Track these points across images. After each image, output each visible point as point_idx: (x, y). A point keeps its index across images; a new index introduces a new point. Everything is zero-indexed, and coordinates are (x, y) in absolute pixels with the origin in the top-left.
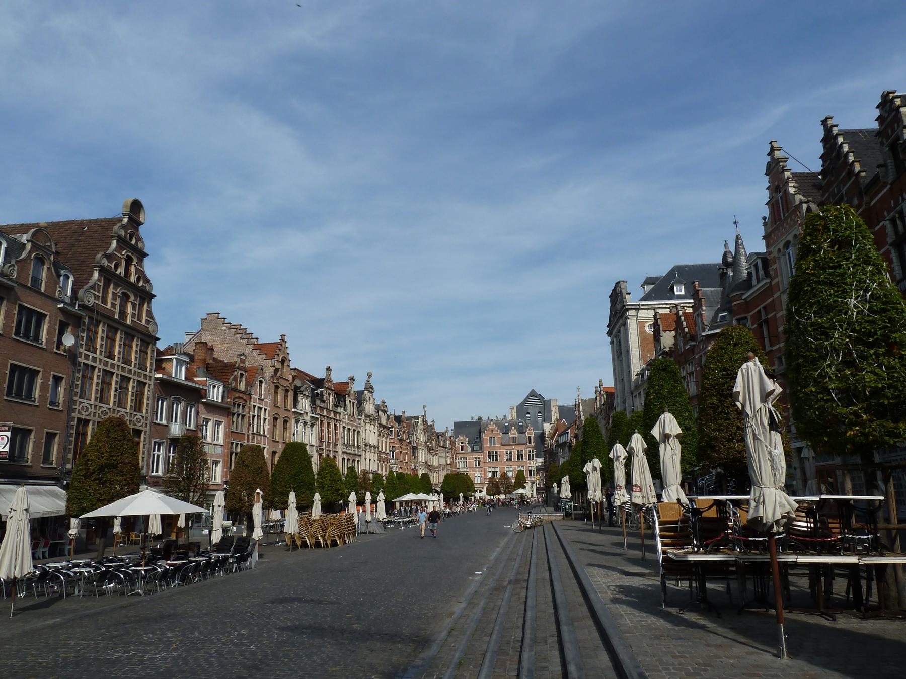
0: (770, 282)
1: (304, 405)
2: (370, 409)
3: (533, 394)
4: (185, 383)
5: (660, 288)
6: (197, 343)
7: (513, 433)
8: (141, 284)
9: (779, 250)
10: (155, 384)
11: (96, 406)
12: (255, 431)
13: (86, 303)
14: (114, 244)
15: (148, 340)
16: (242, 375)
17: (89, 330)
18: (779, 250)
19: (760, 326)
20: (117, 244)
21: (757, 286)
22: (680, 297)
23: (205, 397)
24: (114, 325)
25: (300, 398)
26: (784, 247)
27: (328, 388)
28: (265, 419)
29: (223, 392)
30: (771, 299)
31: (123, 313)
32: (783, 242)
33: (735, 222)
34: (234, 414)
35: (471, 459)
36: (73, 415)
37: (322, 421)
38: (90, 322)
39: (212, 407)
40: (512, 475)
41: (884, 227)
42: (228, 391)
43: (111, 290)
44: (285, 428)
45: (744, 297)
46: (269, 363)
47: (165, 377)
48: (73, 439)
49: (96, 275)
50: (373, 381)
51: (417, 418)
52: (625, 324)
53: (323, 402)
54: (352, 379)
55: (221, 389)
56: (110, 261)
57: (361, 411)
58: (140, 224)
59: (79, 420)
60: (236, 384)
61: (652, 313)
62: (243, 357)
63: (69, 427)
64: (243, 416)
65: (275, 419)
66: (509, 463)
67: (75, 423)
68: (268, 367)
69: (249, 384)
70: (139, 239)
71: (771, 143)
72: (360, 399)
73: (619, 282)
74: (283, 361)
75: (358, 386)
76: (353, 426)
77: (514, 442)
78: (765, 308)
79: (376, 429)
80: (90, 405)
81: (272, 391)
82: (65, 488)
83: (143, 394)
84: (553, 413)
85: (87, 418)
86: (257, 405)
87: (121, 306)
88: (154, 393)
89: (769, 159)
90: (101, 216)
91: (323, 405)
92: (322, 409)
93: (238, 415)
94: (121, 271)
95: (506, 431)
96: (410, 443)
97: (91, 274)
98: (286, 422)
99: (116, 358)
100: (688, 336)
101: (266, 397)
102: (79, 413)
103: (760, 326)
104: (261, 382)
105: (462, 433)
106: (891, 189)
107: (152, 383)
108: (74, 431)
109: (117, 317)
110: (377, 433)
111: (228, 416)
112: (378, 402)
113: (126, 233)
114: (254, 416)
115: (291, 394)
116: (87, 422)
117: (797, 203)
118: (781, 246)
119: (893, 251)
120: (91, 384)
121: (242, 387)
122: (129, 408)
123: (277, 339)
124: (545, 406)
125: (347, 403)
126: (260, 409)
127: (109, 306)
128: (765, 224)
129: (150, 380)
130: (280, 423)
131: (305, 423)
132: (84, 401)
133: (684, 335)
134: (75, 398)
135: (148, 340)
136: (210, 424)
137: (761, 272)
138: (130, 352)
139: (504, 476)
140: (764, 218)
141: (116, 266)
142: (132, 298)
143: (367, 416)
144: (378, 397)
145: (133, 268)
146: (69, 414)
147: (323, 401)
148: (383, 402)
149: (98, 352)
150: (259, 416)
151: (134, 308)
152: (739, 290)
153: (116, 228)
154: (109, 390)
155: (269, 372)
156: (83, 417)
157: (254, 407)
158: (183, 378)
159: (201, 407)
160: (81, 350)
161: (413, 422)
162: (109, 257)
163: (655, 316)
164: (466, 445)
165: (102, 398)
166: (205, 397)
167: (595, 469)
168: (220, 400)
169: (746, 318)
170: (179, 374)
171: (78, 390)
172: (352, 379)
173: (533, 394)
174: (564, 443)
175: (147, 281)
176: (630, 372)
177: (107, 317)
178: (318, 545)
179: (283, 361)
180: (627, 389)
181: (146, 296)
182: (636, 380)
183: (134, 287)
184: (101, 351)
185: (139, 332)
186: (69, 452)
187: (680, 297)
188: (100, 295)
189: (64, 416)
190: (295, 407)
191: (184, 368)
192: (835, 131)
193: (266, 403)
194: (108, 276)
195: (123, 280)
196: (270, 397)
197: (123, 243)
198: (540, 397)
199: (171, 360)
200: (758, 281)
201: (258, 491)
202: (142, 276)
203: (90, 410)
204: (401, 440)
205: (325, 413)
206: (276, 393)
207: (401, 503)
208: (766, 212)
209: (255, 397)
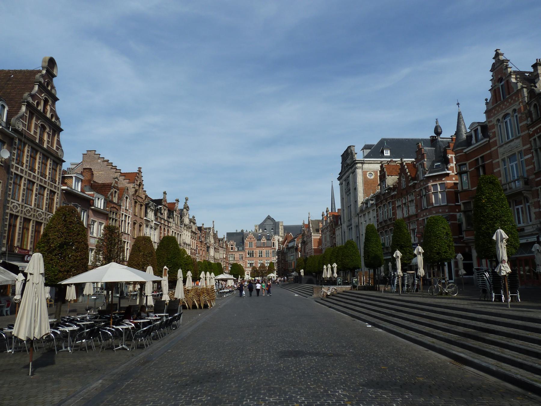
0: (489, 141)
1: (151, 215)
2: (186, 221)
3: (269, 218)
4: (81, 194)
5: (375, 151)
6: (84, 169)
7: (264, 240)
8: (53, 120)
10: (61, 193)
11: (22, 206)
12: (123, 231)
13: (17, 128)
14: (36, 88)
15: (58, 161)
16: (116, 192)
17: (18, 149)
19: (478, 169)
20: (39, 88)
21: (475, 145)
23: (93, 205)
24: (36, 147)
25: (148, 211)
26: (503, 118)
27: (164, 206)
28: (129, 223)
29: (104, 203)
30: (489, 151)
31: (41, 140)
32: (503, 114)
34: (110, 218)
35: (237, 255)
36: (7, 211)
37: (160, 227)
38: (20, 144)
39: (97, 212)
42: (108, 202)
43: (34, 121)
44: (140, 230)
45: (464, 151)
46: (132, 185)
47: (69, 189)
48: (7, 229)
49: (24, 108)
50: (189, 204)
51: (210, 228)
52: (354, 172)
53: (162, 214)
54: (178, 201)
55: (103, 201)
56: (34, 100)
57: (182, 222)
58: (54, 76)
59: (11, 215)
60: (112, 198)
62: (116, 180)
63: (4, 220)
64: (116, 220)
65: (135, 224)
66: (260, 258)
67: (8, 217)
68: (131, 187)
69: (120, 199)
70: (53, 87)
71: (496, 51)
72: (182, 215)
73: (350, 146)
74: (140, 185)
75: (180, 206)
76: (177, 231)
77: (264, 246)
78: (482, 157)
79: (190, 234)
80: (19, 205)
81: (133, 204)
83: (53, 200)
84: (280, 230)
85: (17, 214)
86: (124, 213)
87: (40, 134)
88: (61, 200)
89: (494, 61)
91: (161, 216)
92: (161, 219)
93: (113, 219)
94: (41, 108)
95: (259, 240)
96: (206, 244)
97: (20, 108)
98: (140, 226)
99: (36, 172)
100: (410, 177)
101: (129, 208)
102: (11, 210)
103: (478, 169)
104: (127, 198)
105: (232, 240)
107: (60, 193)
108: (7, 223)
109: (37, 141)
110: (190, 237)
111: (107, 219)
113: (45, 82)
114: (122, 221)
115: (144, 207)
116: (17, 217)
117: (519, 88)
118: (500, 117)
120: (19, 189)
121: (115, 200)
122: (44, 209)
123: (136, 170)
124: (275, 225)
125: (175, 216)
126: (126, 216)
127: (32, 133)
128: (487, 104)
129: (58, 190)
130: (137, 226)
132: (15, 201)
133: (407, 177)
134: (9, 199)
135: (58, 161)
136: (96, 224)
138: (45, 169)
139: (263, 266)
140: (486, 100)
141: (38, 104)
142: (48, 130)
143: (185, 225)
144: (191, 213)
145: (48, 108)
146: (4, 210)
147: (162, 214)
148: (194, 217)
149: (24, 166)
150: (125, 221)
151: (49, 137)
152: (462, 146)
153: (38, 76)
154: (32, 194)
155: (131, 191)
156: (14, 213)
157: (123, 214)
158: (79, 190)
159: (90, 212)
160: (13, 163)
161: (208, 231)
162: (33, 96)
164: (234, 246)
165: (26, 201)
166: (93, 205)
167: (419, 253)
168: (102, 208)
169: (465, 164)
170: (78, 188)
171: (11, 193)
172: (178, 201)
173: (269, 218)
174: (293, 247)
175: (57, 118)
176: (356, 202)
177: (31, 141)
178: (194, 307)
179: (140, 185)
180: (353, 213)
181: (57, 130)
182: (361, 207)
183: (48, 121)
184: (27, 166)
185: (52, 155)
186: (4, 239)
187: (387, 157)
188: (27, 124)
190: (146, 216)
191: (80, 184)
193: (129, 212)
194: (32, 110)
195: (42, 116)
196: (132, 209)
197: (43, 88)
198: (273, 220)
199: (71, 177)
200: (477, 141)
201: (165, 267)
202: (54, 114)
203: (18, 209)
204: (201, 242)
205: (162, 222)
206: (135, 206)
207: (80, 287)
208: (489, 96)
209: (123, 207)
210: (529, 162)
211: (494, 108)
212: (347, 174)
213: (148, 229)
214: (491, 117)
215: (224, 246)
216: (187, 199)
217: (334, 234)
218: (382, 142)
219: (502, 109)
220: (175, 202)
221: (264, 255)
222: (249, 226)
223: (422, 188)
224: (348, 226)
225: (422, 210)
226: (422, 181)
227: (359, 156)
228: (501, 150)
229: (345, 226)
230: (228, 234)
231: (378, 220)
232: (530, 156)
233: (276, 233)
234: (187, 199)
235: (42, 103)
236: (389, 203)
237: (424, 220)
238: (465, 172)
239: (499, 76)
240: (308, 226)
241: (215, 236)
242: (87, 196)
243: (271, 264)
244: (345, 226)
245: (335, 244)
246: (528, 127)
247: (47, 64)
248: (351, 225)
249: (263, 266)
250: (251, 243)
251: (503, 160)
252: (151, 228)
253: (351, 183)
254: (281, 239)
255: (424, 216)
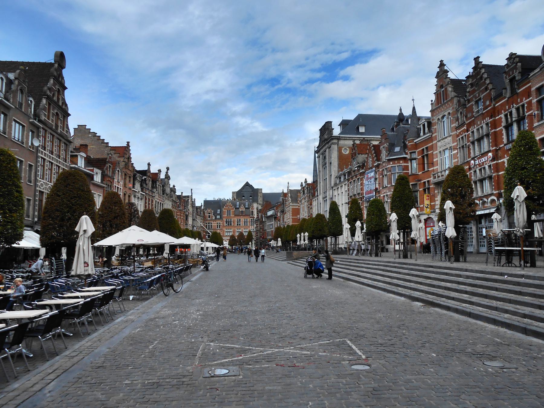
1: (138, 186)
2: (168, 191)
3: (247, 184)
9: (439, 119)
18: (439, 119)
22: (362, 134)
31: (57, 126)
32: (442, 115)
33: (413, 100)
35: (214, 224)
40: (246, 234)
41: (501, 118)
42: (103, 177)
46: (122, 159)
50: (169, 174)
51: (188, 197)
56: (50, 93)
59: (40, 191)
61: (351, 142)
74: (128, 158)
76: (160, 200)
78: (427, 148)
81: (123, 177)
82: (37, 232)
84: (259, 197)
86: (117, 186)
89: (438, 70)
90: (43, 61)
94: (55, 98)
98: (129, 196)
103: (423, 157)
104: (118, 171)
106: (507, 100)
112: (171, 186)
118: (440, 117)
119: (504, 130)
123: (125, 145)
125: (157, 186)
126: (118, 188)
128: (432, 104)
131: (138, 198)
137: (426, 129)
139: (241, 234)
140: (432, 101)
141: (53, 95)
143: (167, 195)
144: (172, 183)
147: (147, 185)
148: (174, 186)
153: (52, 70)
155: (122, 164)
158: (83, 167)
161: (186, 199)
162: (50, 89)
163: (353, 145)
169: (415, 152)
173: (247, 184)
175: (66, 105)
187: (362, 134)
189: (33, 187)
192: (480, 66)
198: (251, 187)
200: (424, 133)
205: (147, 192)
208: (433, 98)
209: (116, 180)
210: (455, 156)
211: (436, 109)
212: (324, 148)
213: (136, 200)
214: (434, 116)
215: (202, 215)
216: (168, 169)
217: (311, 204)
218: (360, 116)
219: (442, 111)
220: (157, 172)
221: (242, 223)
222: (226, 194)
223: (384, 168)
224: (324, 198)
225: (383, 188)
226: (384, 162)
227: (337, 131)
228: (439, 144)
229: (321, 197)
230: (206, 202)
231: (348, 194)
232: (456, 151)
233: (255, 200)
234: (168, 169)
235: (56, 93)
236: (358, 179)
237: (384, 196)
238: (415, 159)
239: (441, 84)
240: (285, 195)
241: (193, 203)
242: (88, 171)
243: (250, 233)
244: (321, 197)
245: (312, 214)
246: (457, 128)
247: (59, 59)
248: (326, 197)
249: (241, 234)
250: (229, 211)
251: (440, 152)
252: (138, 198)
253: (327, 157)
254: (260, 208)
255: (384, 193)
